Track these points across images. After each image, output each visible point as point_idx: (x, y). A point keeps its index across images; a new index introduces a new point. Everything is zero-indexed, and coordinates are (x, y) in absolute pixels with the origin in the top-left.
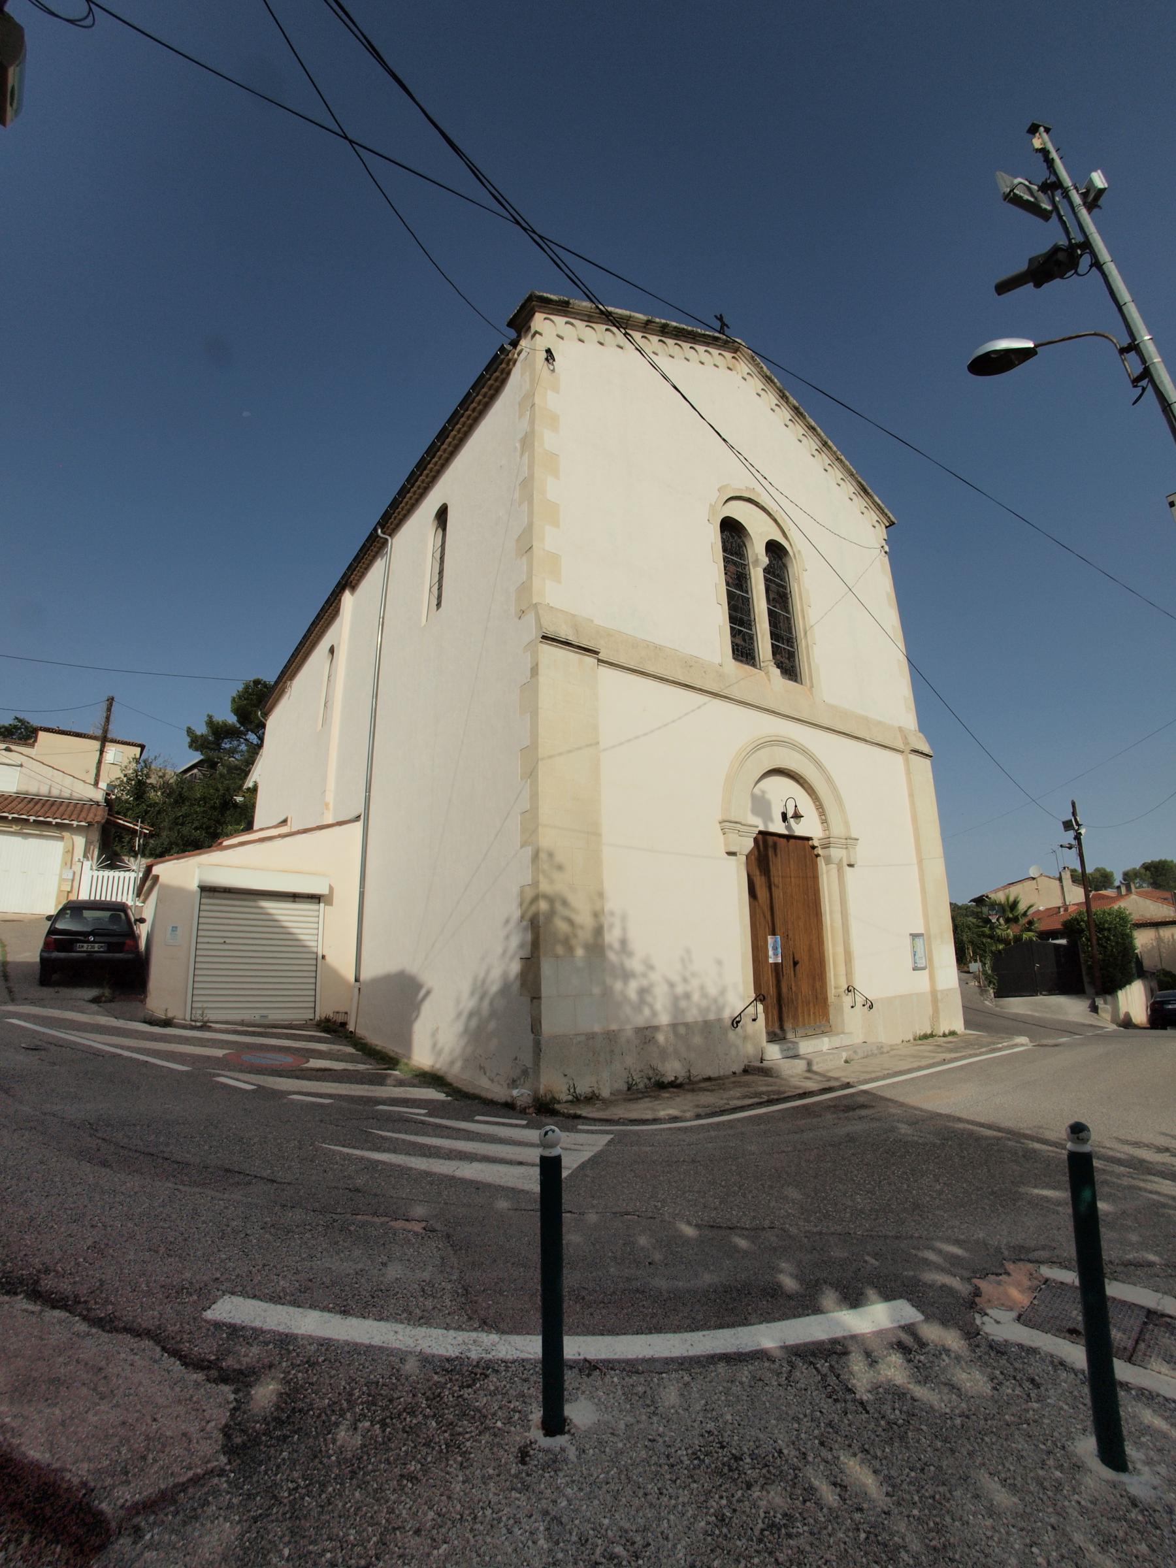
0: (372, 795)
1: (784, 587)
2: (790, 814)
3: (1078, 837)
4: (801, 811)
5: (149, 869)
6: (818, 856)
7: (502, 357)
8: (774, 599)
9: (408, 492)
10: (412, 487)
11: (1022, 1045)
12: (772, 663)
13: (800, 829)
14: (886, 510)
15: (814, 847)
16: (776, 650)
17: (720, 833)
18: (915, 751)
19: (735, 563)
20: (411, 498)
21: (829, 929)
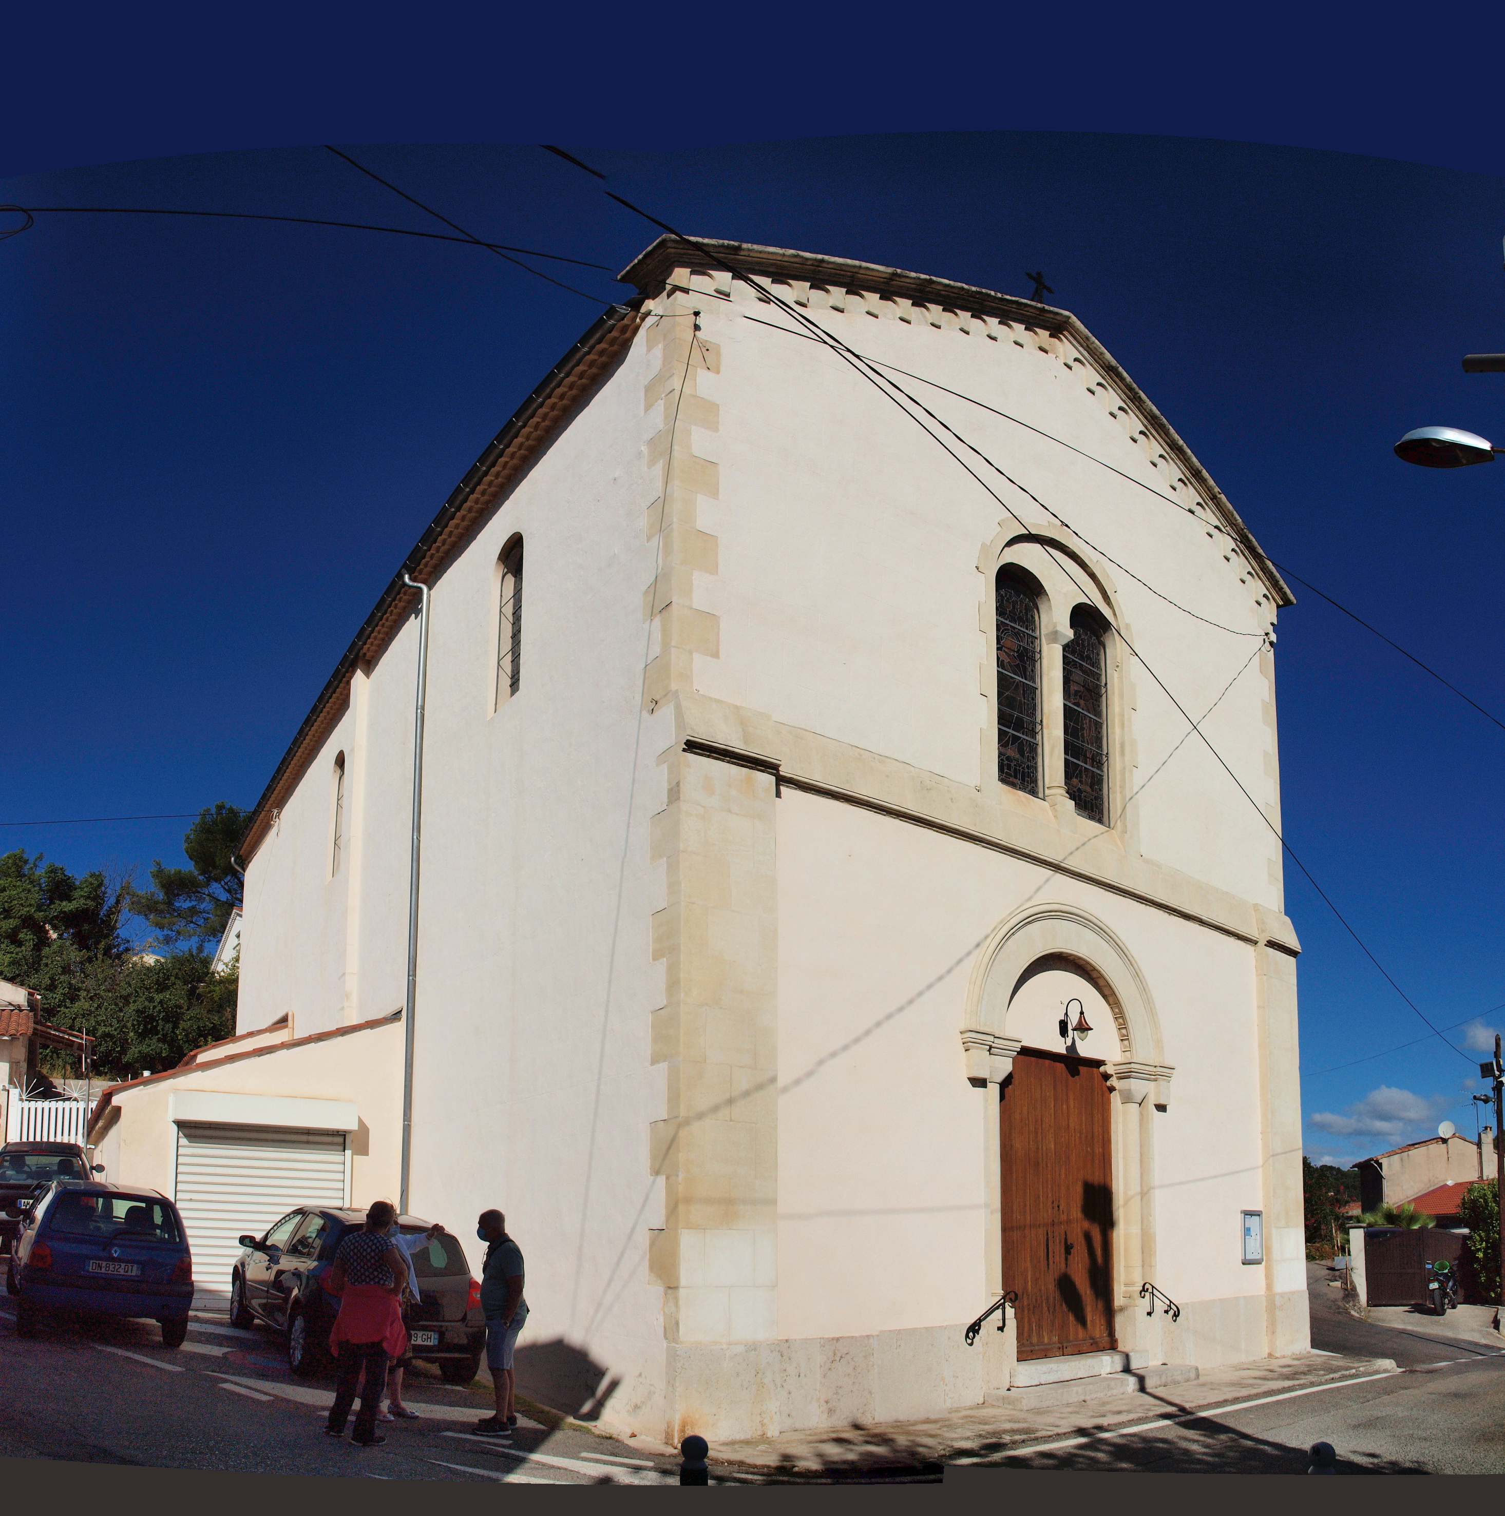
1: (1098, 677)
2: (1074, 1020)
4: (1090, 1020)
5: (107, 1097)
6: (1112, 1089)
7: (612, 322)
8: (1076, 692)
9: (452, 518)
11: (1385, 1371)
13: (1086, 1049)
14: (1282, 582)
15: (1107, 1077)
16: (1071, 771)
17: (962, 1048)
18: (1272, 944)
19: (1017, 634)
21: (1122, 1253)
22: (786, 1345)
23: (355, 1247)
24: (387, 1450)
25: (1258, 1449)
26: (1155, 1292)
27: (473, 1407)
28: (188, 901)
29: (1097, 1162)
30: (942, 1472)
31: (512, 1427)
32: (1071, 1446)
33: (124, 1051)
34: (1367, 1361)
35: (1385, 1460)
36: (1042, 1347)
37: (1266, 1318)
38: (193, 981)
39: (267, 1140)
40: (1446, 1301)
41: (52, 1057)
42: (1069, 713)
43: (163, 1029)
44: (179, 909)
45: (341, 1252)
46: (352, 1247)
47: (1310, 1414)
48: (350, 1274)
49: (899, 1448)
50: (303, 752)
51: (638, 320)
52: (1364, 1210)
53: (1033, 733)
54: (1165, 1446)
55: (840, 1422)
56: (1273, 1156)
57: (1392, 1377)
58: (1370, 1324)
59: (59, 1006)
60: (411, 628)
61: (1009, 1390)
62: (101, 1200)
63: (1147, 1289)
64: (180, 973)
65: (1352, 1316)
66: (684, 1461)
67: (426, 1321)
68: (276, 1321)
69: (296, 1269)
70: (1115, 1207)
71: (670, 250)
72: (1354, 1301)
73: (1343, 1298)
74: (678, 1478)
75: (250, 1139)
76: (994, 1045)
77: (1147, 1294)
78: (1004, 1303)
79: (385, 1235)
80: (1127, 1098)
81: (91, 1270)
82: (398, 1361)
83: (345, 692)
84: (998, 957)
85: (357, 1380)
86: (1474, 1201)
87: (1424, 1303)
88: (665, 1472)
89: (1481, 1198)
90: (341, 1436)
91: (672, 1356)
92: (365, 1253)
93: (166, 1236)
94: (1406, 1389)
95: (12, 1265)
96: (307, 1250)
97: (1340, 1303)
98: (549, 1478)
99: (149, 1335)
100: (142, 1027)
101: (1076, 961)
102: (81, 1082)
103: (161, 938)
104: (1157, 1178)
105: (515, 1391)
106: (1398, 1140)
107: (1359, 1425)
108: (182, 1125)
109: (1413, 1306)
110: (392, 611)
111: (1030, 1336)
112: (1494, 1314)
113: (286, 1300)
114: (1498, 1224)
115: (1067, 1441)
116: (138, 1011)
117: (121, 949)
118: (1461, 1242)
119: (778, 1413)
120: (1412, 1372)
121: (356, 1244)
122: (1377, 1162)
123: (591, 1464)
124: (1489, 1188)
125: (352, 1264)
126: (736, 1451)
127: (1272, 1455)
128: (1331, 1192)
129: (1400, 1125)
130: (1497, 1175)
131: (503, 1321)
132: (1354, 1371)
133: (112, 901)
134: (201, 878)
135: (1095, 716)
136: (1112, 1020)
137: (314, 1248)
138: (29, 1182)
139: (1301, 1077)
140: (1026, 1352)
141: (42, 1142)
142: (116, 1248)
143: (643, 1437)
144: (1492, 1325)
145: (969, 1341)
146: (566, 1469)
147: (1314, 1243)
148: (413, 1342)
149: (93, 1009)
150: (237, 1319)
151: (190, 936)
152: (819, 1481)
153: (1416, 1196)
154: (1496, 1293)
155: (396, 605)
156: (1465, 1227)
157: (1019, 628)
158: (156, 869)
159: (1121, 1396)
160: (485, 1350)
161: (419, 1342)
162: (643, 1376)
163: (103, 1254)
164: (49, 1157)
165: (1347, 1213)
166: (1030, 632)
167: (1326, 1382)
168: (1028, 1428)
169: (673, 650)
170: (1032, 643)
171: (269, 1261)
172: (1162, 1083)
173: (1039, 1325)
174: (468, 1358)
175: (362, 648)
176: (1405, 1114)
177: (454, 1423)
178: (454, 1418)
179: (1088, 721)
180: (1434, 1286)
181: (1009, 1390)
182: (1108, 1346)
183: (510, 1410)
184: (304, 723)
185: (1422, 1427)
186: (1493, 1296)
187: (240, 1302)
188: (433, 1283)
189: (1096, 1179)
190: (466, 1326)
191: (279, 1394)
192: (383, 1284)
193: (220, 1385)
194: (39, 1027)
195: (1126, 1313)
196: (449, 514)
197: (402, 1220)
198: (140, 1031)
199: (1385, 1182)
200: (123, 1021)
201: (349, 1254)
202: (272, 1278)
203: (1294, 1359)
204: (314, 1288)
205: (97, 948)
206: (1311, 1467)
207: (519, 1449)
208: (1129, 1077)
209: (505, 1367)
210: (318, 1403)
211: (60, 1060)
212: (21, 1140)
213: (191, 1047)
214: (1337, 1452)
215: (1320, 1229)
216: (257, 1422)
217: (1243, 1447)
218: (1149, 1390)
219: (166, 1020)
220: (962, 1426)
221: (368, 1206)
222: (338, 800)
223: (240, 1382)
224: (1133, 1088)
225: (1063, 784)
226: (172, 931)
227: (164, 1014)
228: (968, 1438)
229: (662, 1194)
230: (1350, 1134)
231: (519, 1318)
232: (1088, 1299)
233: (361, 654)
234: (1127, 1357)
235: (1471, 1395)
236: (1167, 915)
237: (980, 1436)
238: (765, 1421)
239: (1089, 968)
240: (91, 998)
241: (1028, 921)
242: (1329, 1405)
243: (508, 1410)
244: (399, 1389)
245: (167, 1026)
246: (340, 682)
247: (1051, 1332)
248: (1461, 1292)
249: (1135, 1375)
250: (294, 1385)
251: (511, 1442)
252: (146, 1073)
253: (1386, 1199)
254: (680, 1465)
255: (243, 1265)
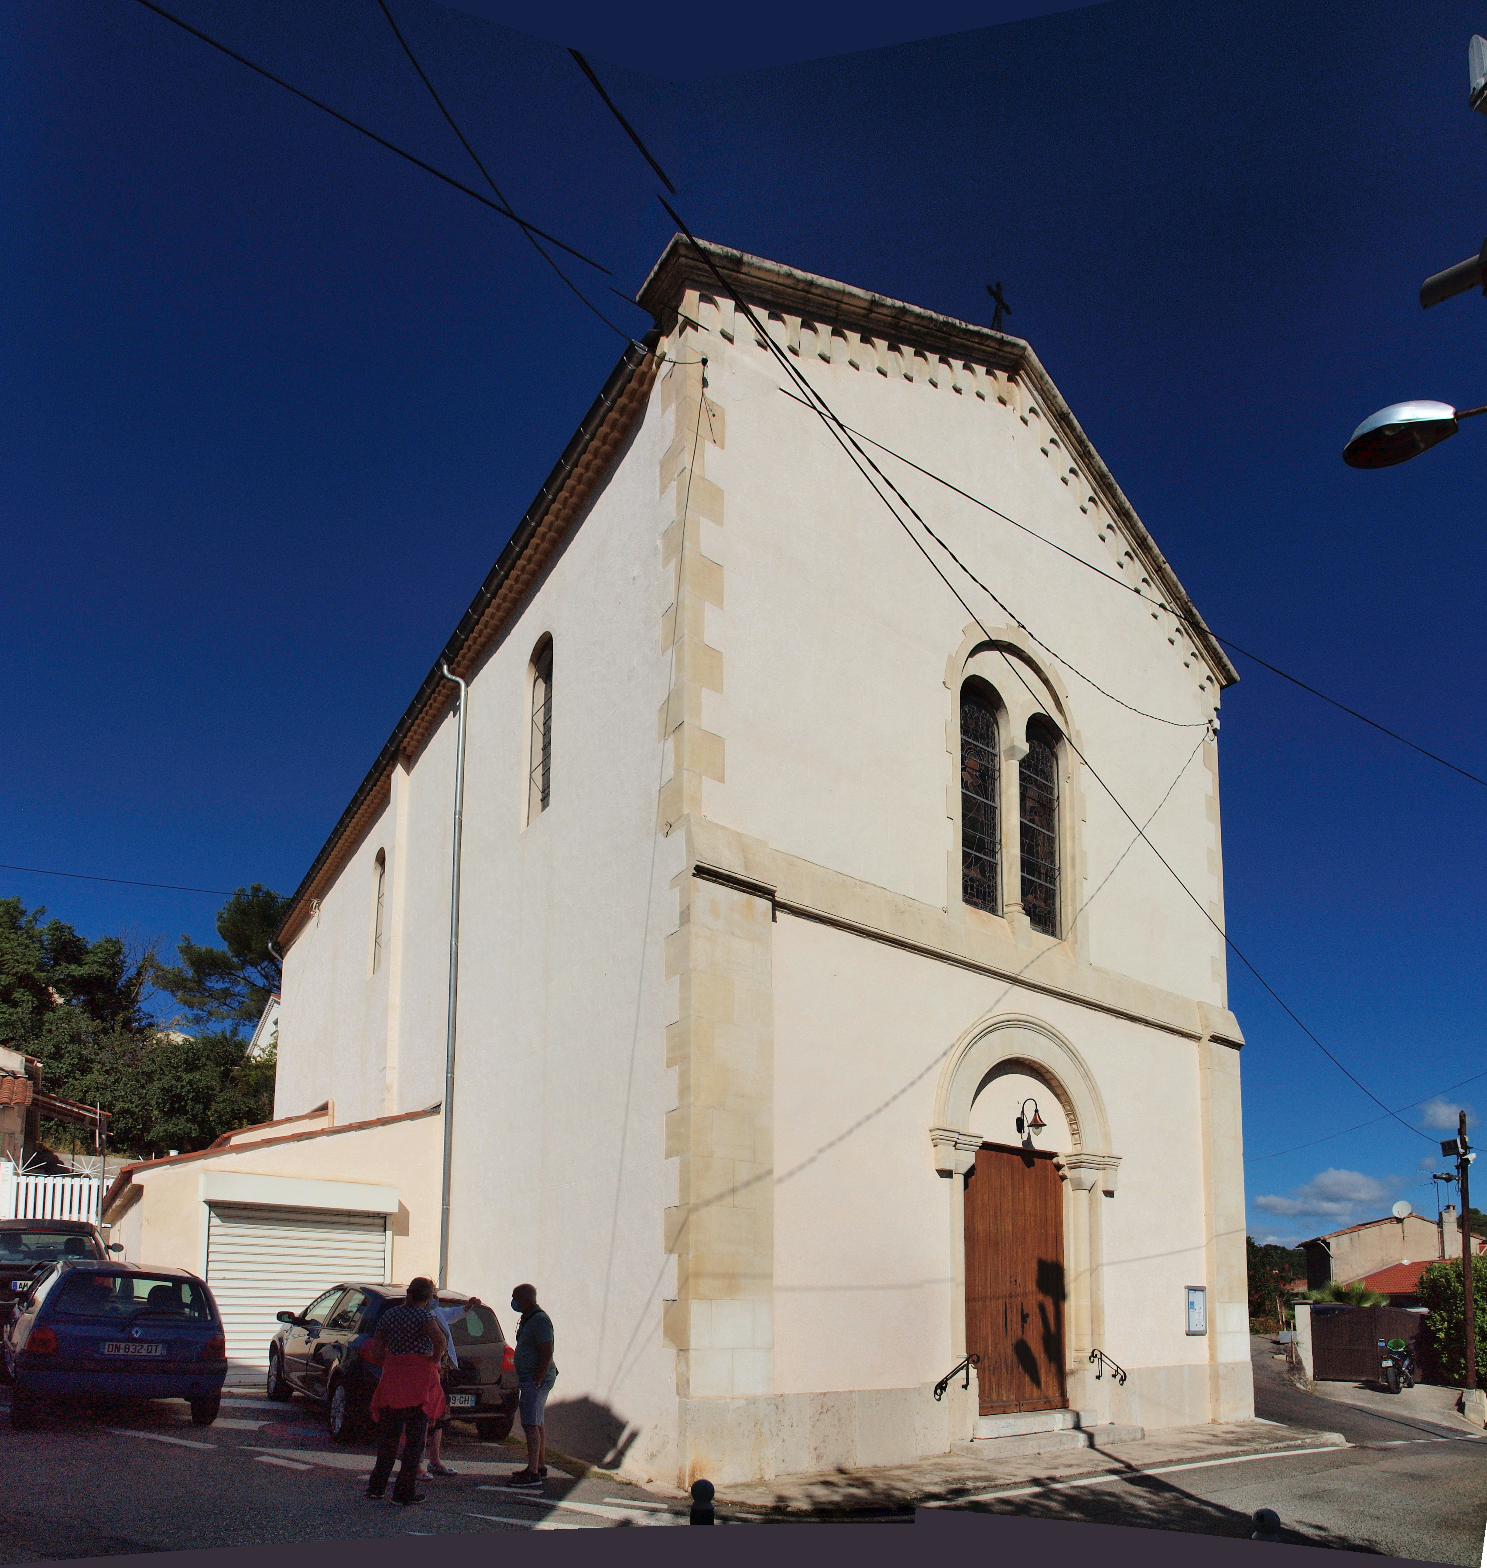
0: (456, 1077)
1: (1050, 790)
2: (1029, 1118)
3: (1463, 1165)
5: (126, 1176)
6: (1063, 1178)
8: (1032, 808)
9: (488, 606)
10: (494, 596)
11: (1333, 1445)
12: (1020, 908)
13: (1040, 1143)
14: (1226, 659)
15: (1059, 1167)
16: (1026, 887)
17: (931, 1144)
18: (1215, 1039)
20: (493, 616)
21: (1073, 1322)
22: (781, 1399)
23: (396, 1320)
24: (427, 1507)
25: (1201, 1510)
26: (1103, 1357)
27: (507, 1462)
28: (220, 982)
29: (1050, 1242)
30: (914, 1514)
31: (543, 1478)
32: (1027, 1494)
33: (146, 1129)
34: (1313, 1433)
35: (1333, 1534)
36: (1001, 1404)
37: (1209, 1386)
38: (226, 1063)
39: (306, 1221)
40: (1402, 1379)
41: (57, 1131)
42: (1025, 831)
43: (192, 1110)
44: (210, 989)
45: (382, 1324)
46: (392, 1320)
47: (1254, 1480)
48: (391, 1345)
49: (876, 1491)
50: (344, 844)
51: (654, 367)
52: (1310, 1288)
53: (993, 853)
54: (1113, 1499)
55: (826, 1467)
56: (1216, 1236)
57: (1341, 1451)
58: (1317, 1398)
59: (66, 1077)
60: (449, 725)
61: (972, 1441)
62: (119, 1281)
63: (1096, 1355)
64: (212, 1055)
65: (1298, 1388)
66: (694, 1503)
67: (463, 1384)
68: (316, 1392)
69: (337, 1342)
70: (1066, 1281)
71: (683, 260)
72: (1299, 1374)
73: (1289, 1371)
74: (689, 1518)
75: (289, 1220)
76: (959, 1141)
77: (1096, 1360)
78: (968, 1364)
79: (425, 1308)
80: (1078, 1186)
81: (106, 1352)
82: (438, 1423)
83: (386, 786)
84: (962, 1063)
85: (398, 1442)
86: (1434, 1281)
87: (1376, 1380)
88: (677, 1514)
89: (1442, 1277)
90: (381, 1498)
91: (684, 1410)
92: (405, 1325)
93: (196, 1314)
94: (1356, 1464)
95: (4, 1352)
96: (348, 1323)
97: (1285, 1376)
98: (576, 1523)
99: (176, 1414)
100: (168, 1106)
101: (1032, 1065)
102: (94, 1158)
103: (190, 1017)
104: (1106, 1254)
105: (545, 1445)
106: (1349, 1221)
107: (1305, 1496)
108: (214, 1205)
109: (1363, 1382)
110: (431, 705)
111: (990, 1394)
112: (1458, 1396)
113: (326, 1371)
114: (1463, 1305)
115: (1024, 1490)
116: (163, 1089)
117: (143, 1024)
118: (1418, 1321)
119: (774, 1459)
120: (1363, 1448)
121: (397, 1317)
122: (1324, 1241)
123: (613, 1508)
124: (1451, 1267)
125: (393, 1335)
126: (737, 1493)
127: (1216, 1517)
128: (1275, 1270)
129: (1350, 1205)
130: (1461, 1255)
131: (534, 1383)
132: (1299, 1442)
133: (133, 971)
134: (235, 960)
135: (1049, 831)
136: (1064, 1116)
137: (354, 1321)
138: (27, 1262)
139: (1245, 1162)
140: (987, 1408)
141: (43, 1220)
142: (137, 1329)
143: (659, 1482)
144: (1456, 1408)
145: (937, 1397)
146: (591, 1514)
147: (1258, 1317)
148: (451, 1405)
149: (109, 1083)
150: (274, 1392)
151: (223, 1018)
152: (809, 1520)
153: (1366, 1275)
154: (1460, 1375)
155: (435, 698)
156: (1423, 1306)
157: (981, 746)
158: (184, 945)
159: (1073, 1451)
160: (518, 1410)
161: (457, 1404)
162: (659, 1428)
163: (121, 1335)
164: (54, 1236)
165: (1292, 1289)
166: (990, 750)
167: (1271, 1451)
168: (989, 1476)
169: (685, 772)
170: (992, 761)
171: (308, 1335)
172: (1110, 1171)
173: (998, 1384)
174: (502, 1417)
175: (402, 741)
176: (1354, 1195)
177: (490, 1477)
178: (489, 1473)
179: (1042, 837)
180: (1388, 1363)
181: (972, 1441)
182: (1060, 1405)
183: (541, 1462)
184: (345, 813)
185: (1374, 1505)
186: (1457, 1377)
187: (278, 1376)
188: (469, 1351)
189: (1049, 1257)
190: (501, 1388)
191: (320, 1462)
192: (423, 1353)
193: (257, 1459)
194: (40, 1098)
195: (1076, 1375)
196: (485, 600)
197: (441, 1294)
198: (166, 1110)
199: (1333, 1262)
200: (146, 1098)
201: (389, 1326)
202: (312, 1351)
203: (1237, 1426)
204: (355, 1359)
205: (114, 1020)
206: (1255, 1533)
207: (550, 1498)
208: (1079, 1167)
209: (537, 1424)
210: (359, 1468)
211: (68, 1134)
212: (16, 1216)
213: (224, 1129)
214: (1282, 1520)
215: (1264, 1304)
216: (297, 1492)
217: (1187, 1507)
218: (1098, 1447)
219: (196, 1100)
220: (931, 1472)
221: (408, 1282)
222: (379, 898)
223: (275, 1453)
224: (1082, 1176)
225: (1019, 901)
226: (203, 1010)
227: (194, 1094)
228: (936, 1483)
229: (676, 1269)
230: (1295, 1215)
231: (549, 1379)
232: (1042, 1363)
233: (401, 748)
234: (1078, 1416)
235: (1431, 1477)
236: (1114, 1018)
237: (947, 1481)
238: (763, 1466)
239: (1043, 1071)
240: (107, 1072)
241: (989, 1030)
242: (1274, 1473)
243: (540, 1463)
244: (438, 1449)
245: (197, 1106)
246: (381, 775)
247: (1009, 1390)
248: (1419, 1372)
249: (1084, 1432)
250: (335, 1452)
251: (542, 1491)
252: (173, 1153)
253: (1334, 1277)
254: (690, 1506)
255: (281, 1340)
